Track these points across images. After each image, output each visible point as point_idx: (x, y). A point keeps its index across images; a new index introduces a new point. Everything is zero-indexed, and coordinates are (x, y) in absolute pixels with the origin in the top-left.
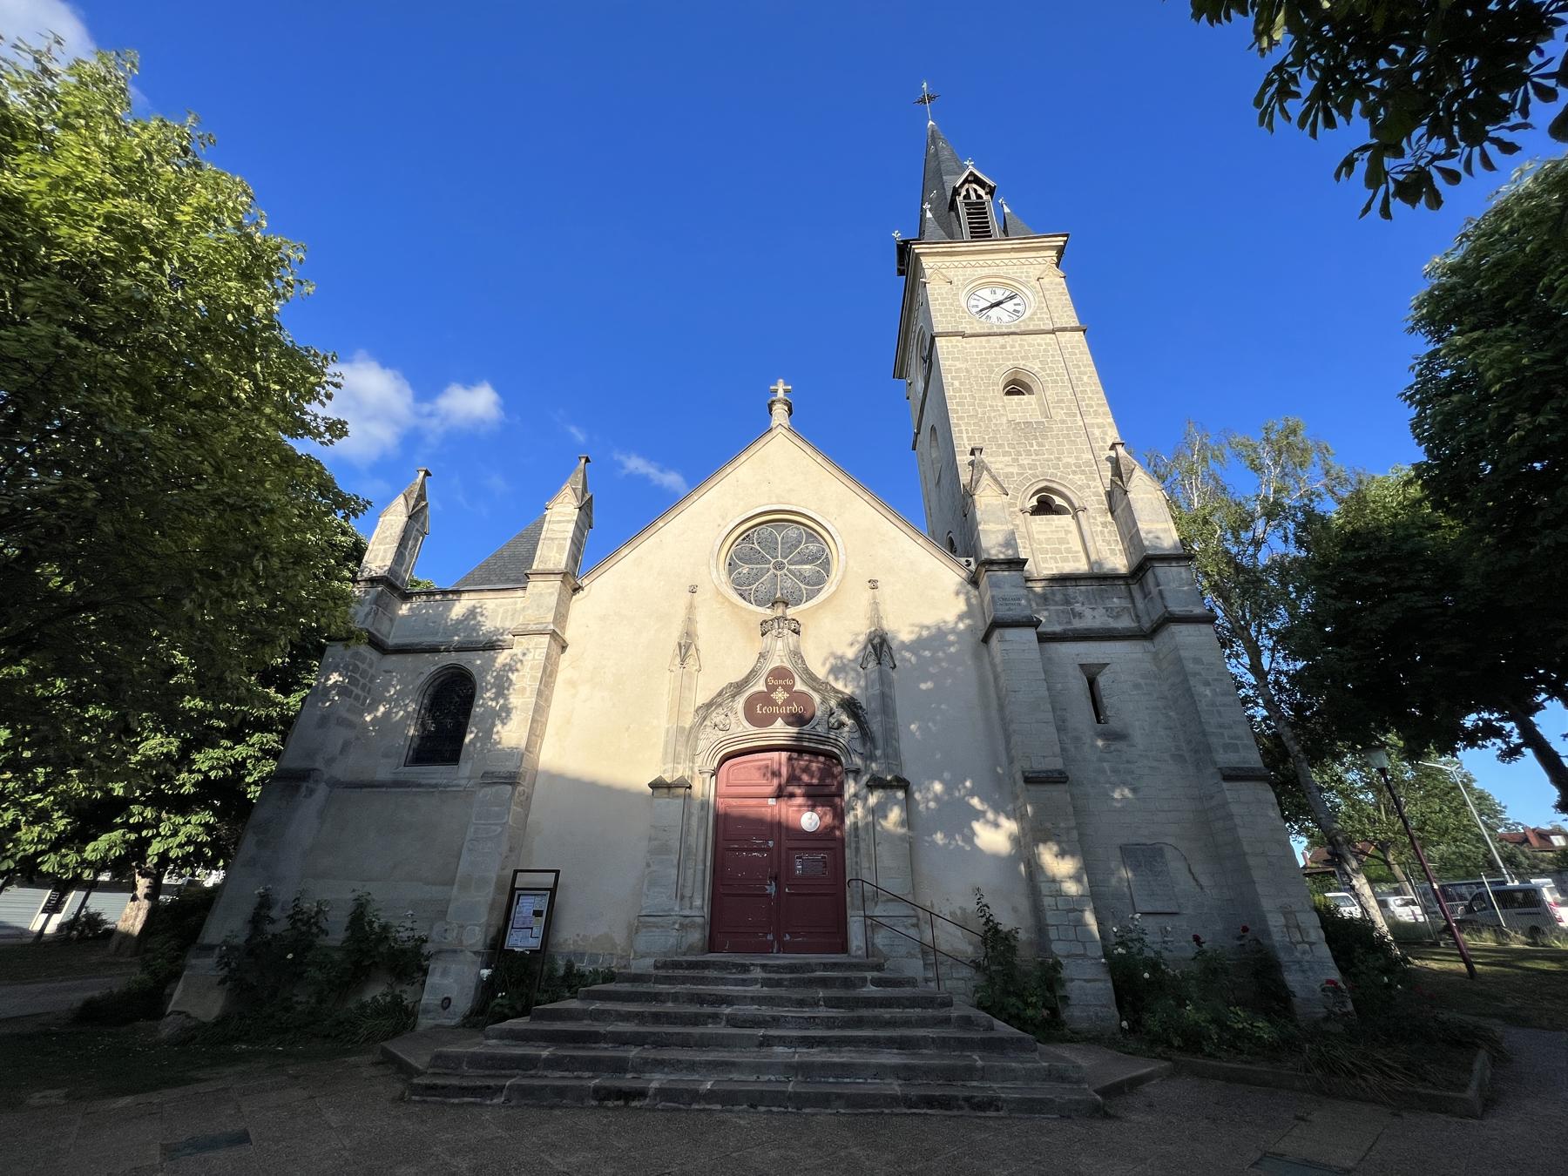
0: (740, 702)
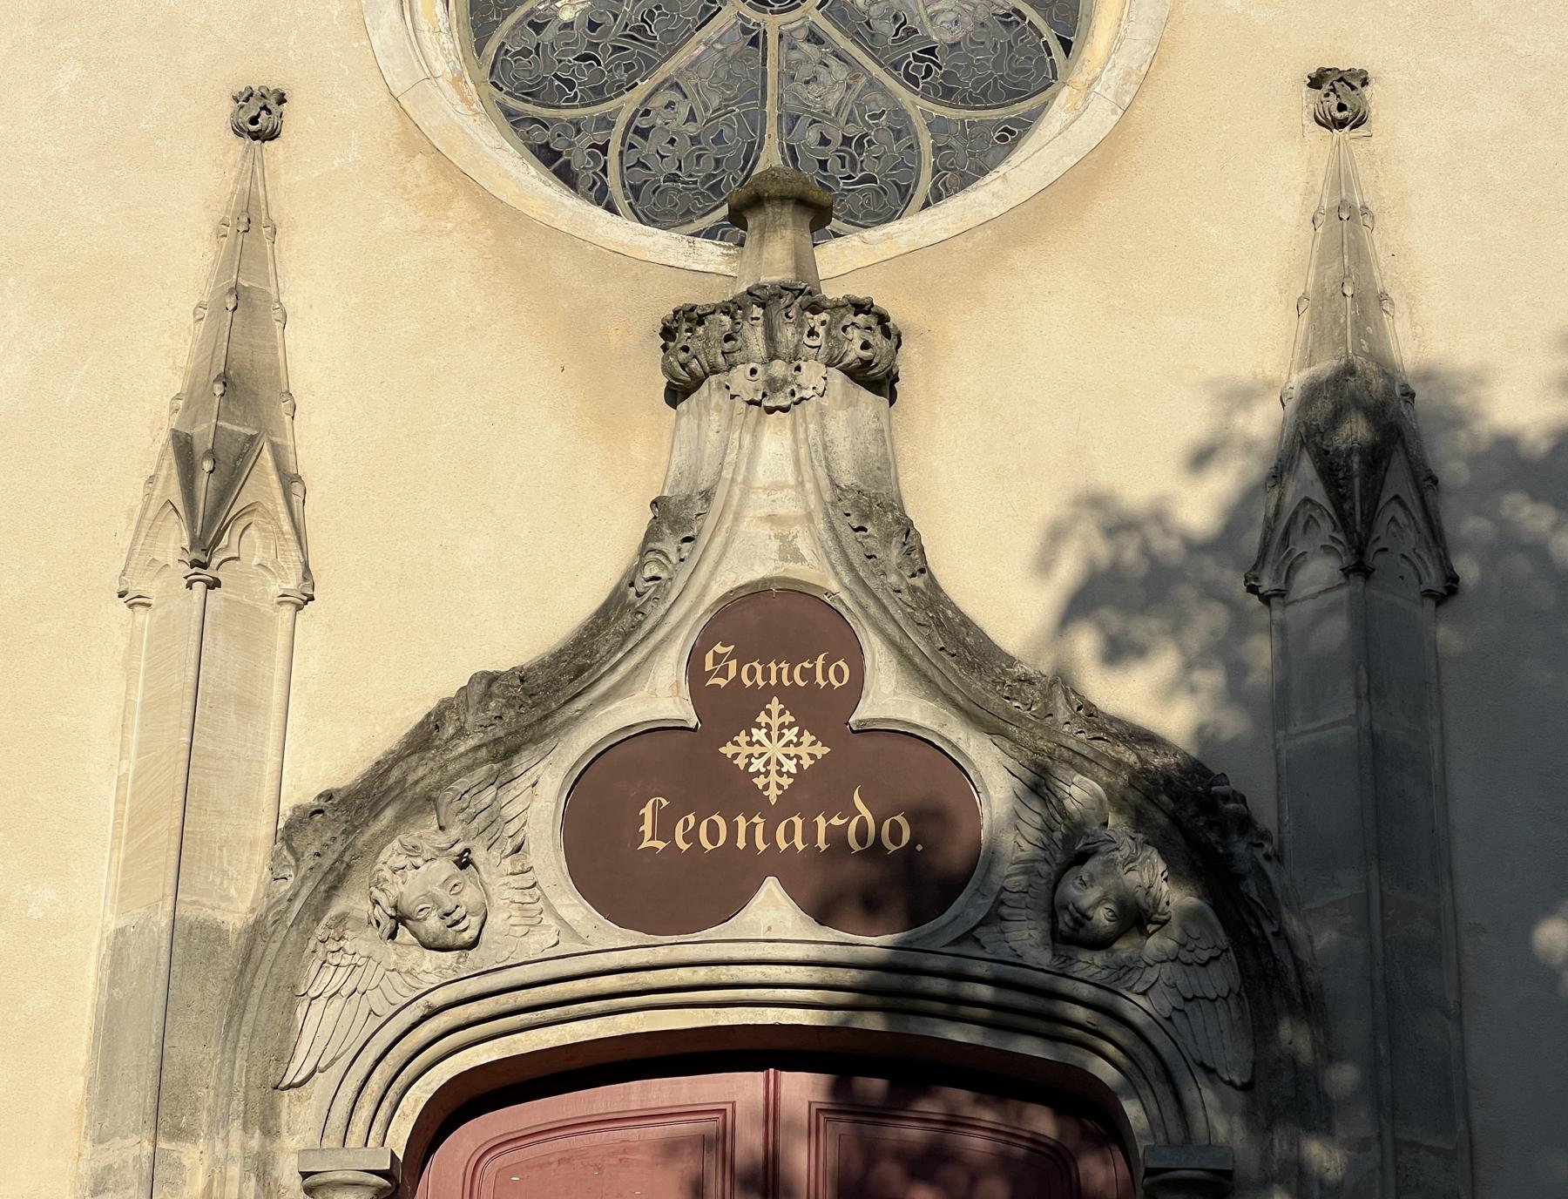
0: (540, 793)
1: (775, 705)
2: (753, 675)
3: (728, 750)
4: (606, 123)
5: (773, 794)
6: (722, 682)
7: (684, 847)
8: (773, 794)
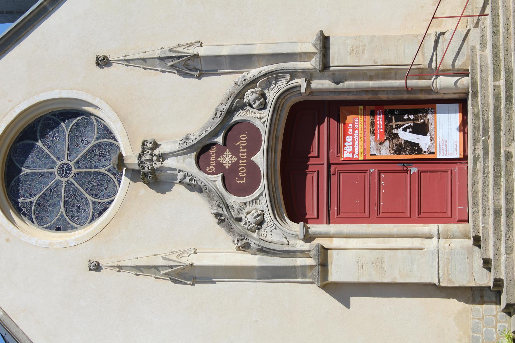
0: (233, 200)
1: (219, 159)
2: (213, 163)
3: (227, 167)
4: (94, 203)
5: (236, 159)
6: (214, 169)
7: (245, 175)
8: (236, 159)
